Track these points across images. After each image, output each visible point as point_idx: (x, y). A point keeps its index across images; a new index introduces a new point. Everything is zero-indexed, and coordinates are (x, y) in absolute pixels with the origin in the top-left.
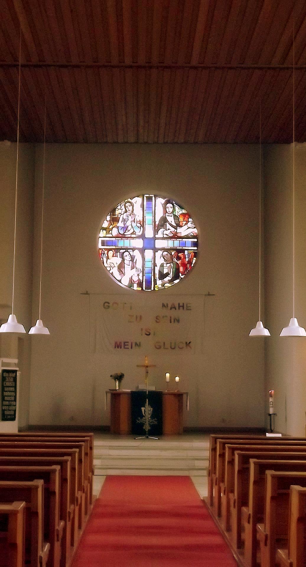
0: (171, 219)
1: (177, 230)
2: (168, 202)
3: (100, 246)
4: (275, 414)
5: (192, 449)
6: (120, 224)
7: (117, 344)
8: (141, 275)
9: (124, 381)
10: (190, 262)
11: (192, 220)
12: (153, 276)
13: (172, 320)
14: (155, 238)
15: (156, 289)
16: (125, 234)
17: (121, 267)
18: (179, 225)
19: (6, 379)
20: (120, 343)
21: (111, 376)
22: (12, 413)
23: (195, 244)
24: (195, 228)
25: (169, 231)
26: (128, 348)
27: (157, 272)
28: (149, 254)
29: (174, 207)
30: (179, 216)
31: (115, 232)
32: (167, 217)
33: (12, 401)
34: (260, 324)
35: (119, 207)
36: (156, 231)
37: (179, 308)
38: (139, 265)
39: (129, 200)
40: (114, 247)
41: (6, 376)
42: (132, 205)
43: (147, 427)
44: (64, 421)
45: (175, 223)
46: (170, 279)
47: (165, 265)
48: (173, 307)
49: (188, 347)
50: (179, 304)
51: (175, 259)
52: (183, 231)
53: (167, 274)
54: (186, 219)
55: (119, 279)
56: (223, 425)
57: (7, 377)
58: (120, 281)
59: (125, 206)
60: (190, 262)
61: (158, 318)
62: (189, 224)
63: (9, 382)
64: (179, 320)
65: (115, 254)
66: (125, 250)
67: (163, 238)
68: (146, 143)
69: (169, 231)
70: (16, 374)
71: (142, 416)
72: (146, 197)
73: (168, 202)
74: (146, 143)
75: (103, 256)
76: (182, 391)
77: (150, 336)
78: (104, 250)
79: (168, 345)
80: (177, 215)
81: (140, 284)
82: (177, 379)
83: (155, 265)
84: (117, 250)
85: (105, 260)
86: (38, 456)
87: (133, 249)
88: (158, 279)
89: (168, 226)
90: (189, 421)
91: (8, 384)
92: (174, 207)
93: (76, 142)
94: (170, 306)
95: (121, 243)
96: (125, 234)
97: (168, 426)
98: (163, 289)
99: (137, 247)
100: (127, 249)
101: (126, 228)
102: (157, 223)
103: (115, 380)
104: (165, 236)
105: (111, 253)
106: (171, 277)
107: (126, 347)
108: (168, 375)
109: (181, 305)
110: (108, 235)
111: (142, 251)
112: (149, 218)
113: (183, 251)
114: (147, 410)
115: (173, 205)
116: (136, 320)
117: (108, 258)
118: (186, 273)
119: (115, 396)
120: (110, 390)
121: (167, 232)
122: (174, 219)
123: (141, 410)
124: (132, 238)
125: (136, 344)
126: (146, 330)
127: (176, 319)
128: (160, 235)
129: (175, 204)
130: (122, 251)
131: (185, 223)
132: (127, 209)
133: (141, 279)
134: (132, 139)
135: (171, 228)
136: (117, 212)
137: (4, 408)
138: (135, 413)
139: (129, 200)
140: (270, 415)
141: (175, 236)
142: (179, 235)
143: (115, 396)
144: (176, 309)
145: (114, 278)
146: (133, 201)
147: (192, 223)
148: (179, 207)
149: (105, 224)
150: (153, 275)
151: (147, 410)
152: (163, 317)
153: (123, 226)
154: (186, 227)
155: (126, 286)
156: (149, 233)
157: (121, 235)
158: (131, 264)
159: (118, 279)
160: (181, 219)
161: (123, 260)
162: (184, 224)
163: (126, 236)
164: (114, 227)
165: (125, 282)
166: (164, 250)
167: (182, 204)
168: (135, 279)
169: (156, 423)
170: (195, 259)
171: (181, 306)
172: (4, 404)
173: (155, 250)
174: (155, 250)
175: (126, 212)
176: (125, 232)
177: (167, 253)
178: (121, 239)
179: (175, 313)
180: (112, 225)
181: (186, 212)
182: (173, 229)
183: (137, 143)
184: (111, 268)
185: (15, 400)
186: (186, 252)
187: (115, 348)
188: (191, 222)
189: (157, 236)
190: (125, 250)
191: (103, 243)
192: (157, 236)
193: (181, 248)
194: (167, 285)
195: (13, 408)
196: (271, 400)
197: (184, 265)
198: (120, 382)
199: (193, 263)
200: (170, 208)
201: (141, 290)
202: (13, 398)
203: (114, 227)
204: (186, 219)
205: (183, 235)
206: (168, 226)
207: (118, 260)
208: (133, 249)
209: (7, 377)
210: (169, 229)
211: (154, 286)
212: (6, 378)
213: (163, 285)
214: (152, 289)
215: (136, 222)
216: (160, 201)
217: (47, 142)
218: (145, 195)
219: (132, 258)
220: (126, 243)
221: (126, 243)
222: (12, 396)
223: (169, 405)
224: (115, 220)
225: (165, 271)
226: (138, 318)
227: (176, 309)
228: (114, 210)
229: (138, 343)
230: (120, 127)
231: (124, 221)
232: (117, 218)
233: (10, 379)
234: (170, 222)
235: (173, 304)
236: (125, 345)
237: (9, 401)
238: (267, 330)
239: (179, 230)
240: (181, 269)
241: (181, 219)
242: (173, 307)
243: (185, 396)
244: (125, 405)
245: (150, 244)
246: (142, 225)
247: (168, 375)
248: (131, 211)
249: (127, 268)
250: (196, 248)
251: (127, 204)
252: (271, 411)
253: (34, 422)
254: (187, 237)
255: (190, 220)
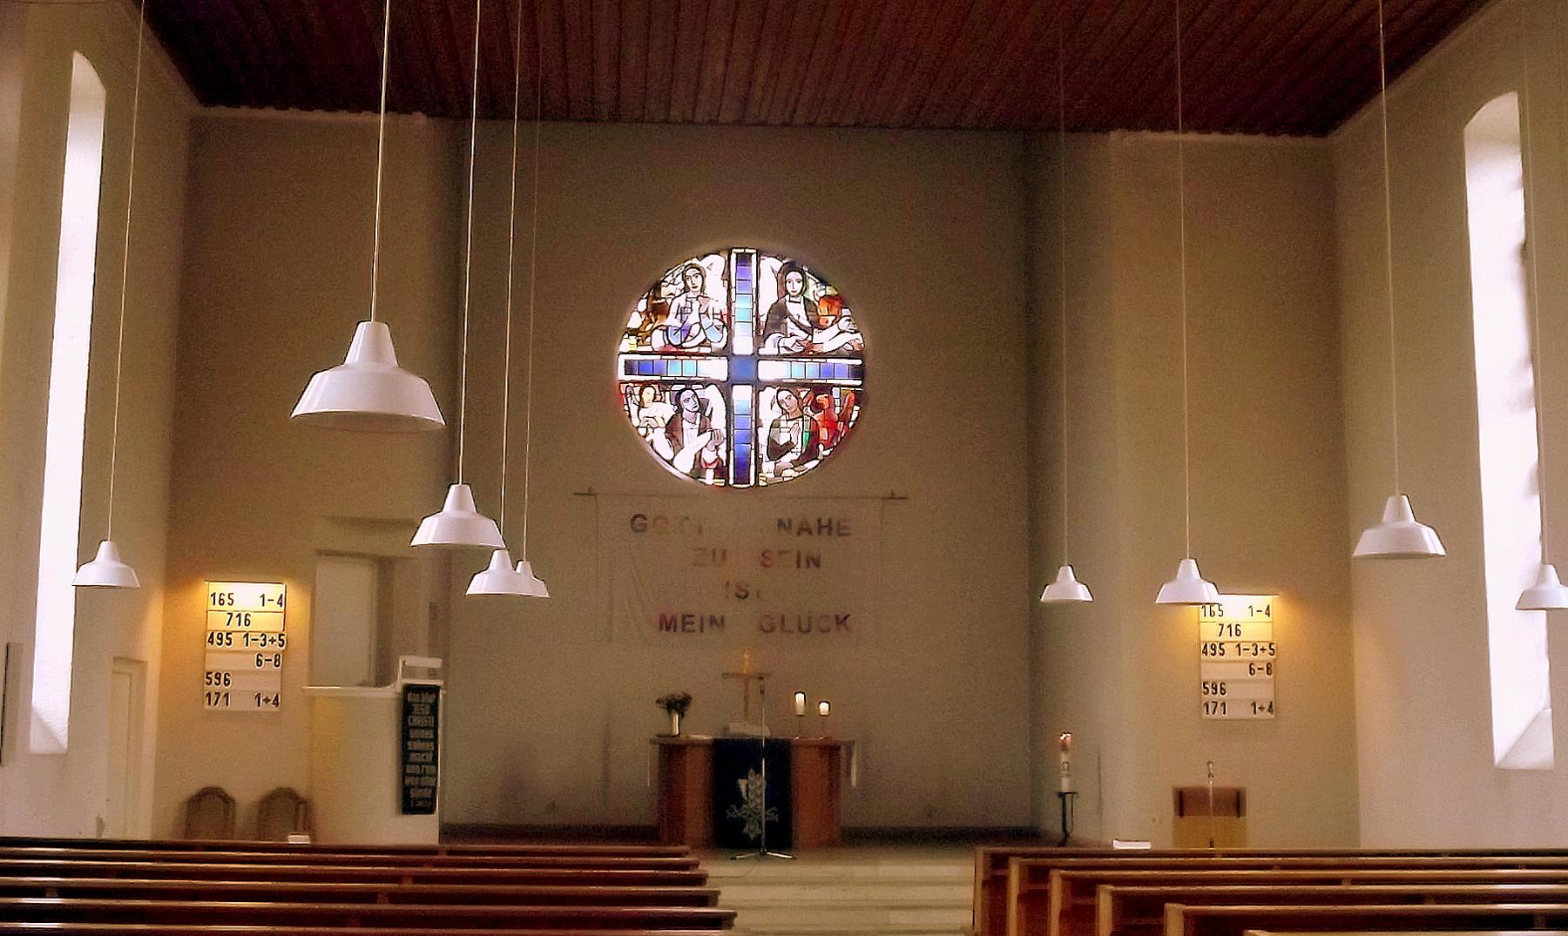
0: (796, 310)
1: (812, 335)
2: (790, 267)
3: (621, 375)
4: (1075, 793)
5: (877, 883)
6: (672, 321)
7: (666, 622)
8: (723, 447)
9: (691, 711)
10: (844, 418)
11: (850, 314)
12: (753, 452)
13: (803, 564)
14: (757, 357)
15: (761, 483)
16: (684, 345)
17: (673, 430)
18: (816, 325)
19: (413, 708)
20: (674, 618)
21: (658, 702)
22: (427, 793)
23: (858, 372)
24: (856, 332)
25: (794, 338)
26: (693, 631)
27: (763, 440)
28: (742, 395)
29: (804, 281)
30: (817, 303)
31: (658, 340)
32: (787, 303)
33: (427, 764)
34: (1067, 571)
35: (669, 279)
36: (760, 336)
37: (819, 532)
38: (718, 422)
39: (695, 261)
40: (658, 378)
41: (414, 700)
42: (701, 273)
43: (753, 830)
44: (535, 815)
45: (808, 320)
46: (796, 457)
47: (783, 424)
48: (804, 529)
49: (842, 628)
50: (819, 521)
51: (809, 408)
52: (827, 340)
53: (789, 447)
54: (835, 311)
55: (668, 454)
56: (923, 822)
57: (416, 703)
58: (670, 462)
59: (683, 273)
60: (844, 418)
61: (767, 555)
62: (843, 324)
63: (421, 715)
64: (819, 561)
65: (661, 395)
66: (683, 386)
67: (779, 357)
68: (763, 124)
69: (794, 338)
70: (437, 698)
71: (739, 801)
72: (737, 254)
73: (790, 267)
74: (763, 124)
75: (629, 399)
76: (839, 736)
77: (747, 600)
78: (631, 385)
79: (791, 624)
80: (812, 299)
81: (721, 471)
82: (824, 707)
83: (758, 424)
84: (665, 385)
85: (634, 409)
86: (445, 904)
87: (706, 383)
88: (766, 458)
89: (791, 326)
90: (854, 812)
91: (417, 721)
92: (804, 281)
93: (592, 118)
94: (795, 525)
95: (676, 369)
96: (684, 345)
97: (805, 822)
98: (779, 485)
99: (714, 377)
100: (689, 384)
101: (685, 331)
102: (763, 319)
103: (670, 712)
104: (783, 351)
105: (649, 393)
106: (799, 454)
107: (688, 627)
108: (800, 698)
109: (824, 522)
110: (641, 349)
111: (726, 389)
112: (742, 306)
113: (826, 389)
114: (753, 786)
115: (802, 273)
116: (713, 559)
117: (641, 406)
118: (835, 444)
119: (671, 752)
120: (658, 736)
121: (789, 342)
122: (805, 309)
123: (738, 785)
124: (701, 355)
125: (713, 621)
126: (738, 587)
127: (813, 559)
128: (769, 348)
129: (807, 273)
130: (677, 387)
131: (831, 319)
132: (689, 283)
133: (723, 456)
134: (727, 116)
135: (797, 331)
136: (665, 291)
137: (408, 781)
138: (723, 794)
139: (695, 261)
140: (1062, 795)
141: (808, 352)
142: (817, 349)
143: (671, 752)
144: (810, 533)
145: (656, 455)
146: (704, 263)
147: (850, 320)
148: (817, 281)
149: (635, 321)
150: (753, 447)
151: (753, 786)
152: (780, 553)
153: (680, 325)
154: (835, 330)
155: (687, 475)
156: (743, 344)
157: (674, 349)
158: (698, 422)
159: (666, 458)
160: (823, 310)
161: (680, 410)
162: (830, 324)
163: (686, 350)
164: (657, 328)
165: (683, 464)
166: (780, 385)
167: (826, 275)
168: (709, 456)
169: (776, 818)
170: (856, 408)
171: (825, 528)
172: (408, 771)
173: (758, 386)
174: (758, 386)
175: (686, 290)
176: (685, 342)
177: (789, 393)
178: (674, 357)
179: (808, 544)
180: (651, 322)
181: (836, 293)
182: (803, 335)
183: (739, 123)
184: (650, 430)
185: (435, 762)
186: (836, 391)
187: (661, 629)
188: (848, 318)
189: (762, 351)
190: (683, 386)
191: (629, 368)
192: (762, 351)
193: (824, 381)
194: (789, 473)
195: (431, 782)
196: (1064, 757)
197: (831, 425)
198: (682, 715)
199: (854, 418)
200: (796, 283)
201: (723, 484)
202: (430, 757)
203: (657, 328)
204: (835, 311)
205: (827, 348)
206: (791, 326)
207: (667, 410)
208: (706, 383)
209: (416, 703)
210: (792, 335)
211: (756, 475)
212: (414, 705)
213: (778, 473)
214: (752, 482)
215: (711, 316)
216: (770, 265)
217: (543, 118)
218: (734, 250)
219: (702, 406)
220: (688, 368)
221: (688, 368)
222: (428, 751)
223: (807, 776)
224: (658, 310)
225: (783, 439)
226: (718, 557)
227: (810, 533)
228: (657, 287)
229: (718, 617)
230: (707, 84)
231: (681, 312)
232: (664, 306)
233: (424, 707)
234: (796, 318)
235: (805, 521)
236: (684, 623)
237: (421, 764)
238: (1085, 586)
239: (818, 337)
240: (824, 434)
241: (823, 310)
242: (804, 529)
243: (843, 752)
244: (696, 775)
245: (743, 372)
246: (727, 323)
247: (800, 698)
248: (699, 289)
249: (689, 431)
250: (859, 383)
251: (690, 272)
252: (1065, 785)
253: (461, 816)
254: (837, 354)
255: (845, 312)
